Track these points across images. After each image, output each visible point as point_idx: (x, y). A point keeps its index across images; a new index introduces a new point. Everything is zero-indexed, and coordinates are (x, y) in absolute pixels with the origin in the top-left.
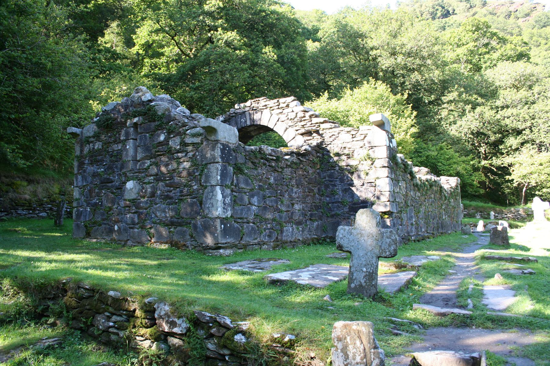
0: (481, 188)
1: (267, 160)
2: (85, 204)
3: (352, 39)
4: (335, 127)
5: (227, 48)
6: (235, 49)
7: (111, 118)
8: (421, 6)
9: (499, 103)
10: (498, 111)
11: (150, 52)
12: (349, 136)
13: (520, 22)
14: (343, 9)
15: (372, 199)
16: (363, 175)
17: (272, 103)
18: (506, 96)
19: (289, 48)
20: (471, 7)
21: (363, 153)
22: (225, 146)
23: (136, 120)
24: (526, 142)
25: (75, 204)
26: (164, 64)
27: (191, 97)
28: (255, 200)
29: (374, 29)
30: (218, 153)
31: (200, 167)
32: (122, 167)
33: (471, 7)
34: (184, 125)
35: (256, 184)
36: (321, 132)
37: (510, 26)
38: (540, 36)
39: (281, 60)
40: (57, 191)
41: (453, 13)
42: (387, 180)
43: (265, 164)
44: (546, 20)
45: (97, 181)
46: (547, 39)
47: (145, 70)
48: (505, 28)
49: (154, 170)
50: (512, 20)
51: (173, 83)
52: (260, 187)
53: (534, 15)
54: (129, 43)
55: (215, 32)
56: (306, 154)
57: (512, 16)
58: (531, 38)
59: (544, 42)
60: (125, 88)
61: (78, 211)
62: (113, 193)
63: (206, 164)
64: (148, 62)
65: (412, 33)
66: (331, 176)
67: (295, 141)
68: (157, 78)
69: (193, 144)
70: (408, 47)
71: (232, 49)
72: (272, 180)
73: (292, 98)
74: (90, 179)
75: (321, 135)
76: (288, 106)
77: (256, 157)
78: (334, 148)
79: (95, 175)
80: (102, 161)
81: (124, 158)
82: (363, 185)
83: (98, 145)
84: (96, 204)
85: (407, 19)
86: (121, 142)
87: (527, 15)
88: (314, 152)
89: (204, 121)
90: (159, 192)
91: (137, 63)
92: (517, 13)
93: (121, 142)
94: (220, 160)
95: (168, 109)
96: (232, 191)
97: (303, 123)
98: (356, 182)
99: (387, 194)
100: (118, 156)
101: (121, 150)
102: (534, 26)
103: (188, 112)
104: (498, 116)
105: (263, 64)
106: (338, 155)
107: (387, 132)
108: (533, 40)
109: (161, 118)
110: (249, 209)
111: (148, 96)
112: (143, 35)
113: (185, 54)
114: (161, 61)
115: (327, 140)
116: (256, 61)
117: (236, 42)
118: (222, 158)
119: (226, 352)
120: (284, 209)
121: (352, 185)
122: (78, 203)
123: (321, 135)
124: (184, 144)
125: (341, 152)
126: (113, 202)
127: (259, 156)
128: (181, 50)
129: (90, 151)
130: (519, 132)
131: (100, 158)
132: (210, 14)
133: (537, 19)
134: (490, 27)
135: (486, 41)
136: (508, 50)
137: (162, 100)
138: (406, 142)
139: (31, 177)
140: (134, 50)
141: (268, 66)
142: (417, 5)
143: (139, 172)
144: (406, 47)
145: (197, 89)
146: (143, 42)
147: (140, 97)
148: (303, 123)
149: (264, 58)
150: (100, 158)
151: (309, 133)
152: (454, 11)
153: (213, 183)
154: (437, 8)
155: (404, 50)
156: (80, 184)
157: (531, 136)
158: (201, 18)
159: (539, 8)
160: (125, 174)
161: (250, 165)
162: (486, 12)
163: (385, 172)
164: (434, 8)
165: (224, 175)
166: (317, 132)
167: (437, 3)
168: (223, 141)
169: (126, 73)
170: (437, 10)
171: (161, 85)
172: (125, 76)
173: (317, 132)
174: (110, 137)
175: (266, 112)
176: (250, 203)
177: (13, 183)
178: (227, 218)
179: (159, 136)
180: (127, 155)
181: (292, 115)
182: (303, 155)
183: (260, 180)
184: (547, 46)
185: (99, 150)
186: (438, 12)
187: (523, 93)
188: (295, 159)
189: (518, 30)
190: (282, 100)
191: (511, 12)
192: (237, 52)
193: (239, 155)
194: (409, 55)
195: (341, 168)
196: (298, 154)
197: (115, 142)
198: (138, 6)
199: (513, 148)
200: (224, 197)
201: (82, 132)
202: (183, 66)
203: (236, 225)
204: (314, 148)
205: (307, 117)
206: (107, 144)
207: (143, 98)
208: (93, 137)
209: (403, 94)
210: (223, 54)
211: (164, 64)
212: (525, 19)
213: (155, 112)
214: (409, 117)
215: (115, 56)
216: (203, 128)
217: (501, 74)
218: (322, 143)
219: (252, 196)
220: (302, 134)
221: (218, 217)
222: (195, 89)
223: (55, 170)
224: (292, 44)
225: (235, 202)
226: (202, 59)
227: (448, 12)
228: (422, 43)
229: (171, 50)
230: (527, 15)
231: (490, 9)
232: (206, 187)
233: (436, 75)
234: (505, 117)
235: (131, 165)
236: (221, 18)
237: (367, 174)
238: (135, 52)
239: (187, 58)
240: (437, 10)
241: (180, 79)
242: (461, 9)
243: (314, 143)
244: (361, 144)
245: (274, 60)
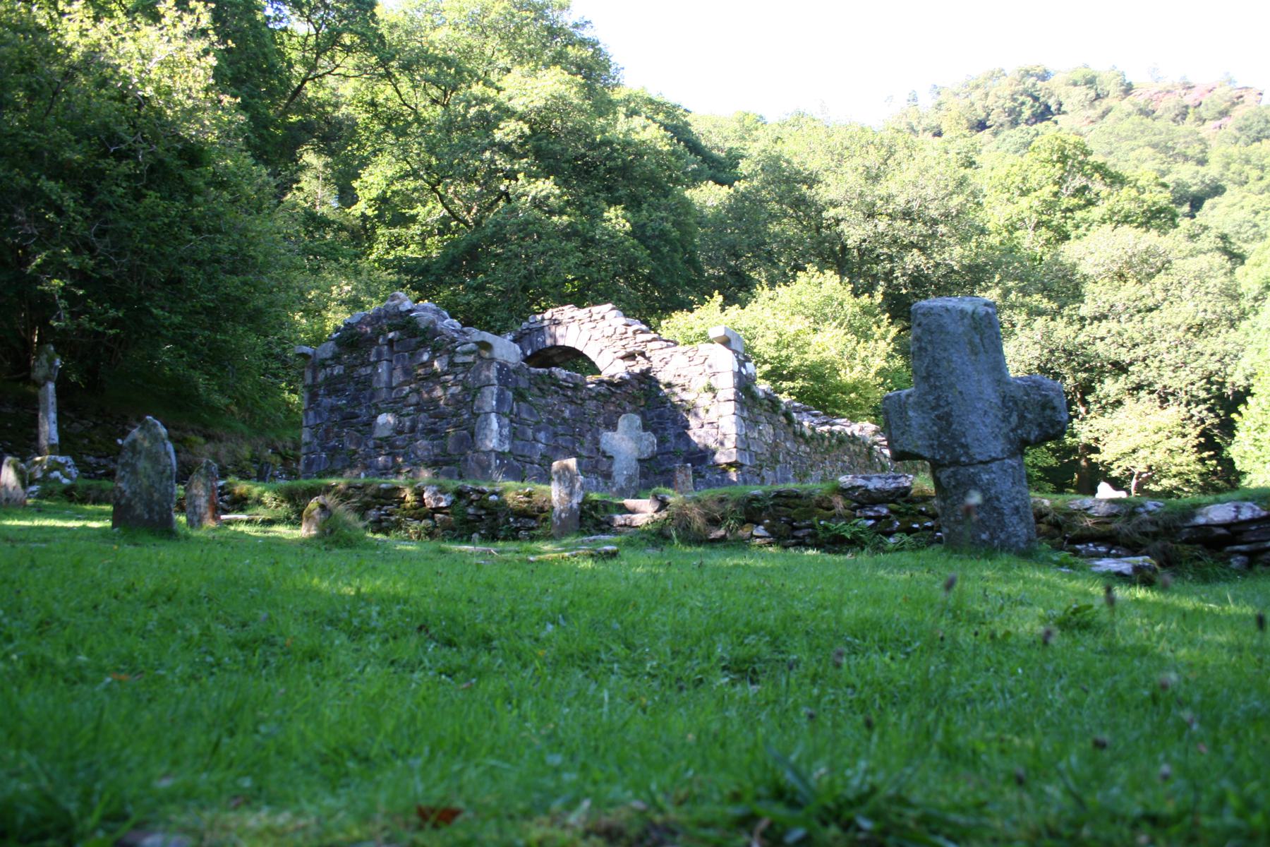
0: (1048, 481)
1: (560, 387)
2: (319, 449)
3: (790, 185)
4: (668, 347)
5: (536, 211)
6: (551, 212)
7: (357, 334)
8: (987, 95)
9: (1086, 310)
10: (1084, 326)
11: (388, 216)
12: (685, 359)
13: (1207, 130)
14: (788, 118)
15: (714, 446)
16: (701, 413)
17: (582, 313)
18: (1095, 297)
19: (657, 209)
20: (1098, 97)
21: (703, 382)
22: (502, 366)
23: (391, 335)
24: (1139, 387)
25: (304, 450)
26: (417, 238)
27: (468, 304)
28: (542, 436)
29: (833, 164)
30: (493, 373)
31: (472, 392)
32: (372, 397)
33: (1098, 97)
34: (453, 341)
35: (544, 417)
36: (647, 355)
37: (1182, 140)
38: (1248, 162)
39: (638, 232)
40: (248, 455)
41: (1059, 109)
42: (734, 418)
43: (557, 392)
44: (1262, 125)
45: (336, 417)
46: (1262, 168)
47: (378, 250)
48: (1170, 144)
49: (413, 399)
50: (1189, 124)
51: (433, 278)
52: (549, 421)
53: (1238, 113)
54: (347, 196)
55: (513, 182)
56: (623, 383)
57: (1190, 117)
58: (1227, 166)
59: (1255, 173)
60: (347, 288)
61: (308, 459)
62: (359, 431)
63: (479, 388)
64: (383, 235)
65: (909, 173)
66: (660, 416)
67: (612, 367)
68: (401, 266)
69: (464, 364)
70: (901, 201)
71: (546, 212)
72: (567, 414)
73: (610, 306)
74: (325, 415)
75: (648, 359)
76: (603, 318)
77: (544, 382)
78: (663, 377)
79: (333, 409)
80: (344, 390)
81: (375, 385)
82: (702, 426)
83: (338, 370)
84: (334, 447)
85: (901, 144)
86: (370, 364)
87: (1224, 113)
88: (635, 382)
89: (476, 335)
90: (420, 426)
91: (362, 235)
92: (1201, 108)
93: (370, 364)
94: (496, 382)
95: (433, 322)
96: (511, 421)
97: (624, 342)
98: (693, 422)
99: (733, 437)
100: (366, 382)
101: (371, 375)
102: (1237, 140)
103: (458, 326)
104: (1082, 338)
105: (604, 241)
106: (669, 385)
107: (734, 351)
108: (1232, 170)
109: (424, 332)
110: (533, 447)
111: (408, 305)
112: (374, 180)
113: (456, 218)
114: (411, 232)
115: (656, 364)
116: (591, 234)
117: (552, 199)
118: (499, 379)
119: (483, 512)
120: (584, 453)
121: (687, 427)
122: (309, 449)
123: (648, 359)
124: (452, 364)
125: (674, 382)
126: (359, 445)
127: (548, 381)
128: (450, 211)
129: (326, 378)
130: (1120, 368)
131: (341, 386)
132: (505, 148)
133: (1242, 123)
134: (1090, 153)
135: (1079, 181)
136: (1123, 199)
137: (425, 309)
138: (866, 385)
139: (210, 431)
140: (359, 208)
141: (613, 243)
142: (977, 94)
143: (395, 402)
144: (897, 199)
145: (480, 288)
146: (374, 194)
147: (396, 306)
148: (624, 342)
149: (606, 229)
150: (341, 386)
151: (631, 356)
152: (1061, 105)
153: (488, 410)
154: (1021, 99)
155: (891, 206)
156: (311, 422)
157: (1150, 375)
158: (488, 154)
159: (1250, 98)
160: (376, 405)
161: (536, 391)
162: (1129, 108)
163: (731, 407)
164: (1014, 100)
165: (500, 401)
166: (642, 354)
167: (1021, 88)
168: (500, 359)
169: (347, 261)
170: (1023, 104)
171: (410, 282)
172: (346, 266)
173: (642, 354)
174: (355, 358)
175: (574, 327)
176: (535, 439)
177: (185, 439)
178: (503, 453)
179: (421, 355)
180: (379, 381)
181: (610, 331)
182: (618, 385)
183: (550, 413)
184: (1263, 184)
185: (339, 375)
186: (1024, 108)
187: (1130, 289)
188: (603, 389)
189: (1198, 148)
190: (595, 309)
191: (1187, 107)
192: (555, 219)
193: (520, 378)
194: (906, 214)
195: (674, 406)
196: (610, 383)
197: (363, 365)
198: (366, 128)
199: (1111, 400)
200: (501, 427)
201: (315, 353)
202: (454, 244)
203: (516, 463)
204: (634, 376)
205: (630, 333)
206: (351, 368)
207: (402, 308)
208: (332, 359)
209: (871, 296)
210: (527, 223)
211: (417, 238)
212: (1218, 123)
213: (417, 325)
214: (884, 337)
215: (321, 223)
216: (476, 343)
217: (1094, 249)
218: (648, 370)
219: (539, 430)
220: (623, 358)
221: (492, 450)
222: (476, 289)
223: (244, 422)
224: (663, 201)
225: (514, 435)
226: (488, 231)
227: (1048, 108)
228: (930, 192)
229: (430, 212)
230: (1224, 113)
231: (1141, 101)
232: (478, 415)
233: (956, 255)
234: (1095, 338)
235: (384, 394)
236: (525, 156)
237: (707, 411)
238: (358, 213)
239: (461, 225)
240: (1023, 104)
241: (448, 269)
242: (1075, 102)
243: (637, 370)
244: (700, 369)
245: (626, 233)
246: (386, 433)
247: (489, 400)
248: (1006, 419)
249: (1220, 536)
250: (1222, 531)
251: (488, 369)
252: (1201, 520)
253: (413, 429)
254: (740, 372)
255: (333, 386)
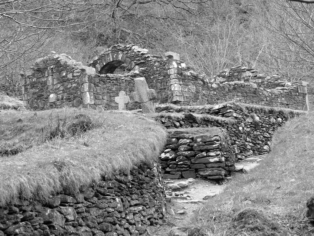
22: (89, 76)
30: (87, 79)
32: (47, 88)
69: (77, 76)
79: (34, 94)
81: (48, 84)
90: (65, 97)
94: (88, 82)
118: (88, 81)
165: (90, 87)
180: (49, 83)
183: (108, 89)
225: (96, 98)
235: (51, 87)
246: (53, 101)
247: (86, 87)
248: (148, 96)
249: (217, 111)
250: (217, 110)
251: (85, 77)
252: (214, 109)
253: (62, 99)
254: (178, 67)
255: (33, 85)
